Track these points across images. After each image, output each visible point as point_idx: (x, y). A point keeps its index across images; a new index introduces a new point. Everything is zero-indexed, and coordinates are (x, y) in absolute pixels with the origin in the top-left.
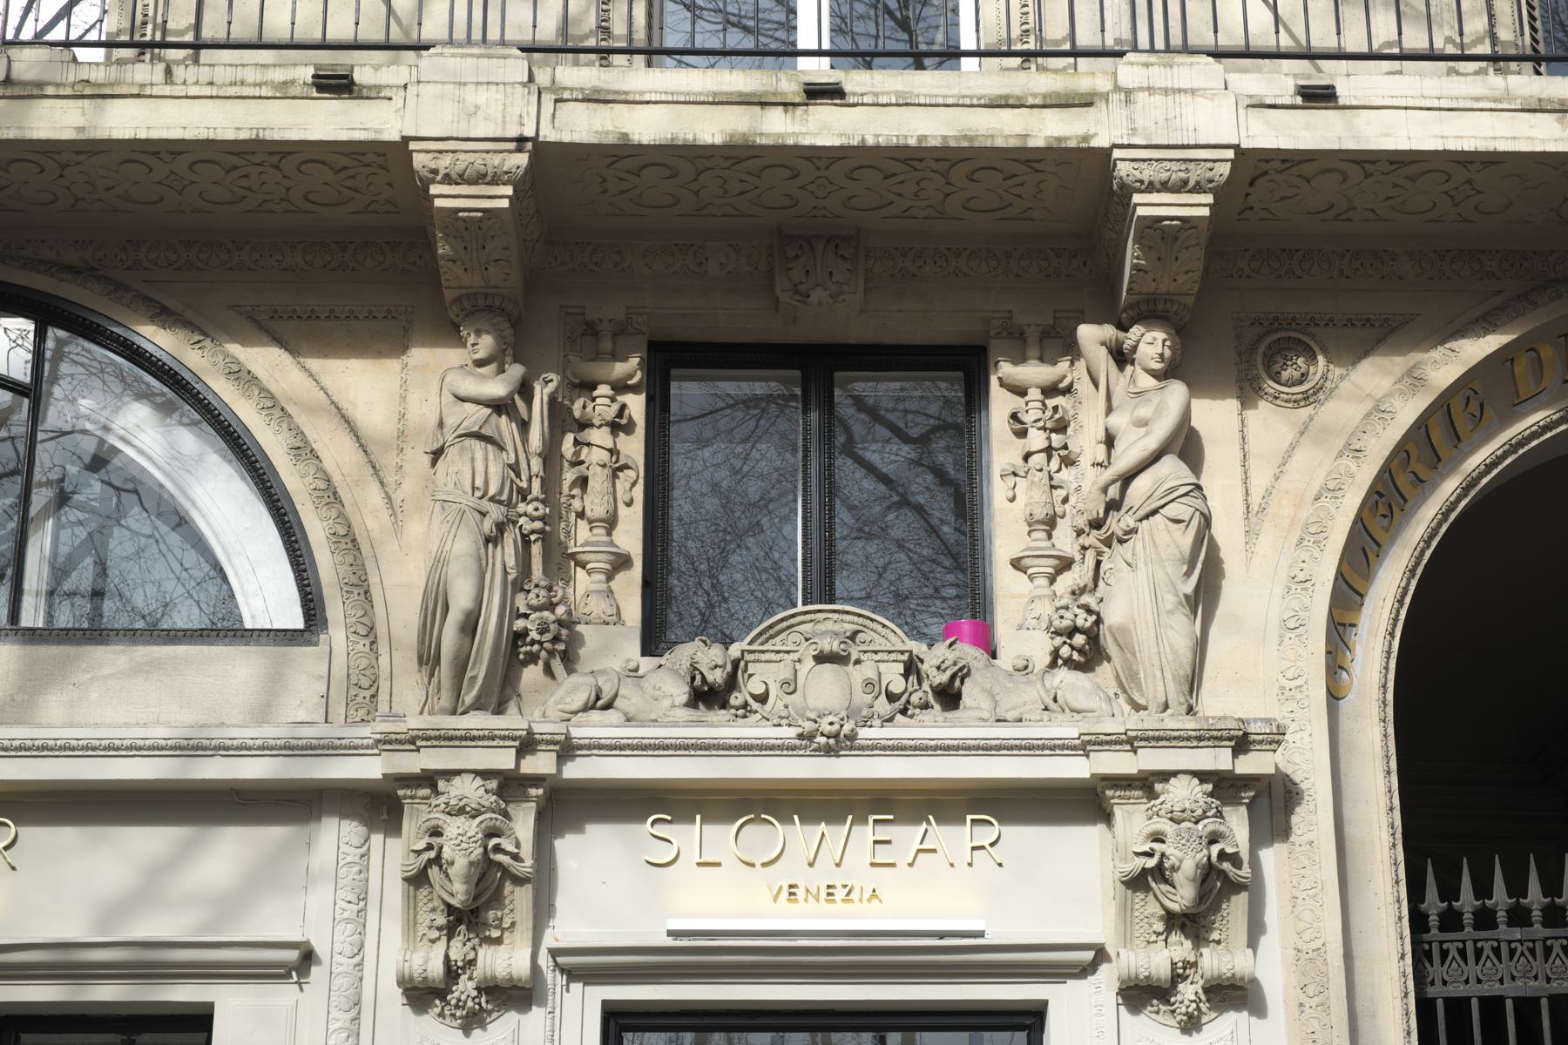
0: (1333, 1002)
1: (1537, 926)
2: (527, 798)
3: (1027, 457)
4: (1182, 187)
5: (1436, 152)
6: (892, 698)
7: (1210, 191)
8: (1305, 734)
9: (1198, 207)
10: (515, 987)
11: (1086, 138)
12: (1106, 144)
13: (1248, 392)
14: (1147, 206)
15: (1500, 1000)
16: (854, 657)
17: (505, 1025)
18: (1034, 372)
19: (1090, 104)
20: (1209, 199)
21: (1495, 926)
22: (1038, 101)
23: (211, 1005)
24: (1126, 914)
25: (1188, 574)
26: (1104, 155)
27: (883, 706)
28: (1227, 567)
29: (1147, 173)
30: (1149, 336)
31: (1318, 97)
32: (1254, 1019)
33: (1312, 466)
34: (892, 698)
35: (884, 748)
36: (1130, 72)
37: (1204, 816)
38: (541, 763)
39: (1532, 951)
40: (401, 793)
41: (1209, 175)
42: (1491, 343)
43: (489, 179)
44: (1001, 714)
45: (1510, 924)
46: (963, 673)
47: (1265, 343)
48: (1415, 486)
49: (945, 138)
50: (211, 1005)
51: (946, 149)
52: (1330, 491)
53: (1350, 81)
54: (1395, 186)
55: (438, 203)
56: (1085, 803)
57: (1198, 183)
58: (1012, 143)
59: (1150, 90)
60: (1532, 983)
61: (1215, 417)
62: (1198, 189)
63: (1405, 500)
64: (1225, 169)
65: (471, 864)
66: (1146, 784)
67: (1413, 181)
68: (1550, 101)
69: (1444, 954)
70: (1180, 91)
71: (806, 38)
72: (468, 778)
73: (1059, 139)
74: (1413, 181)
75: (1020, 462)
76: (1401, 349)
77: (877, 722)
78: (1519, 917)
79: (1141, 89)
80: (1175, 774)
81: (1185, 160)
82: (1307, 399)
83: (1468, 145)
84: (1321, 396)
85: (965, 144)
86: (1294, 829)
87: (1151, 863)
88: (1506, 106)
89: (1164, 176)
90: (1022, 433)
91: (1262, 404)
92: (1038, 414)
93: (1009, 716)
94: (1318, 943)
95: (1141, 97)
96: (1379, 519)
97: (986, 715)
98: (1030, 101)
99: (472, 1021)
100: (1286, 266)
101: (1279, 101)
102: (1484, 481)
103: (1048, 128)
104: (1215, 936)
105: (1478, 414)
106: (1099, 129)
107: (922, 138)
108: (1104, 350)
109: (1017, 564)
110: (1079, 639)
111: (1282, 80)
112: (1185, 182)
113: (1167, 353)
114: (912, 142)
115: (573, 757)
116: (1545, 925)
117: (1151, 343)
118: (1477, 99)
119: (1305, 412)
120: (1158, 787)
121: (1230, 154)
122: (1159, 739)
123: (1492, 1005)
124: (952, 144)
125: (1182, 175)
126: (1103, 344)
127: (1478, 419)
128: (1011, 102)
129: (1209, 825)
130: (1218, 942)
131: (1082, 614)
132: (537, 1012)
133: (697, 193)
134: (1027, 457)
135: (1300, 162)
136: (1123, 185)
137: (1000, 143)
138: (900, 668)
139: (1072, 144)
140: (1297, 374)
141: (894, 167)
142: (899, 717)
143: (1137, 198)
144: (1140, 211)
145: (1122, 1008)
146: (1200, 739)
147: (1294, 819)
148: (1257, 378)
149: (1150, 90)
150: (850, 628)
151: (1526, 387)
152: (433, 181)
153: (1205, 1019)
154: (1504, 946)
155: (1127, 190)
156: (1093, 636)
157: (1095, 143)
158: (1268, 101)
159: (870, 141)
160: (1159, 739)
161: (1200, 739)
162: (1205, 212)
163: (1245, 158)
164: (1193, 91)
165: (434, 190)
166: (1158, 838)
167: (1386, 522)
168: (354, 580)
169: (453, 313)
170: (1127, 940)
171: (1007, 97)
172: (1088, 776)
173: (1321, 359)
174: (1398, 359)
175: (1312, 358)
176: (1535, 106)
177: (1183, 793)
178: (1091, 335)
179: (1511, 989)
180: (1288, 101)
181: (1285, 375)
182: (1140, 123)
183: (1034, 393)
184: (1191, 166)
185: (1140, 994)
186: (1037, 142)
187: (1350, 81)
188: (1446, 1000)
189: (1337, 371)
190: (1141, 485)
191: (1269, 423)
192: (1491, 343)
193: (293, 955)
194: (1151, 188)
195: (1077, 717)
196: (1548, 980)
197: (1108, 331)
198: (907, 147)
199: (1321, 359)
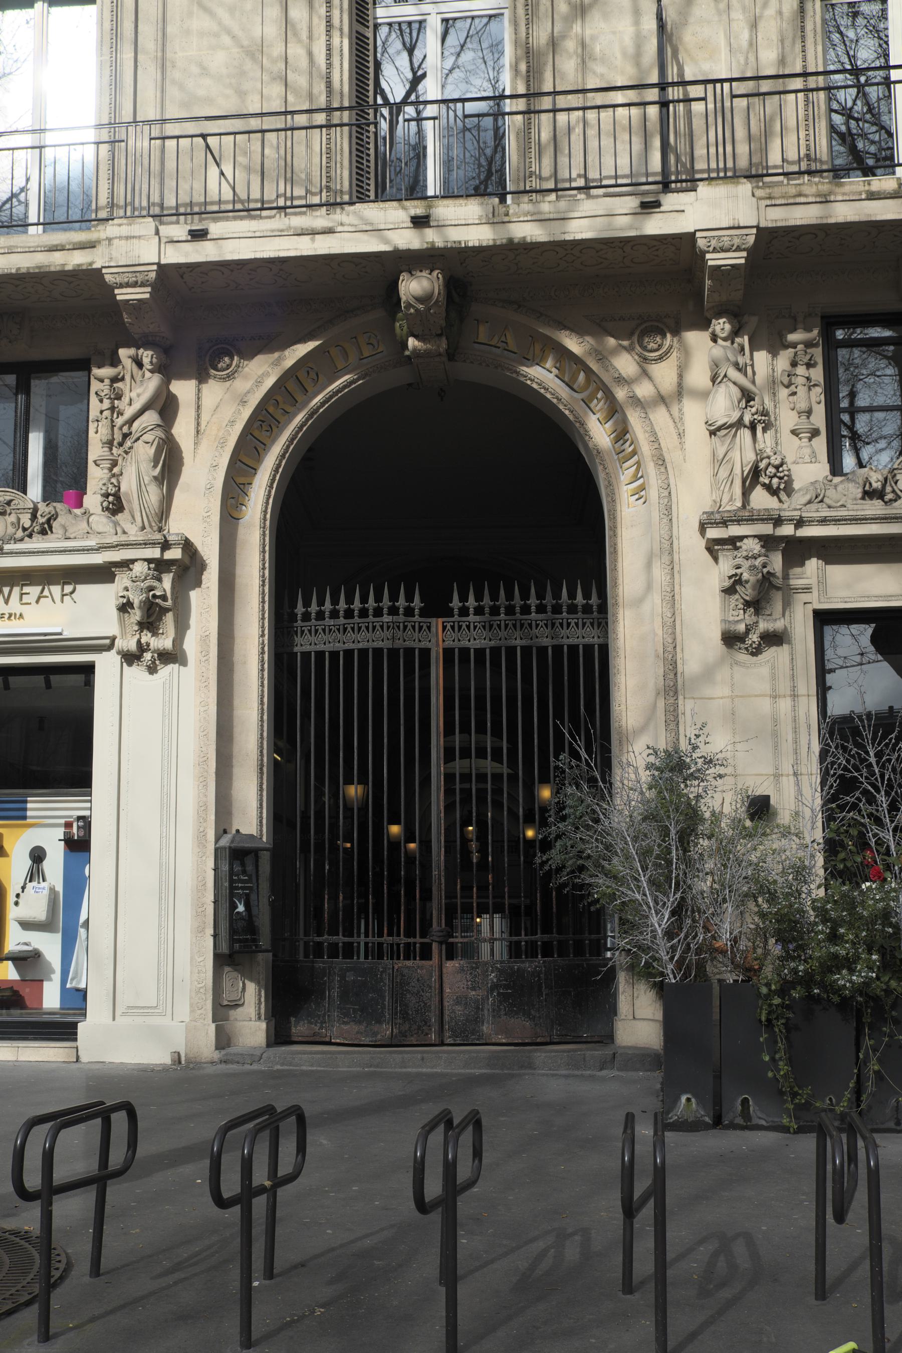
0: (211, 659)
1: (342, 618)
2: (169, 571)
3: (102, 412)
4: (135, 285)
5: (251, 259)
6: (24, 529)
7: (744, 250)
8: (209, 538)
9: (738, 259)
10: (167, 653)
11: (91, 264)
12: (692, 230)
13: (202, 377)
14: (714, 260)
15: (323, 652)
16: (8, 512)
17: (166, 671)
18: (106, 372)
19: (94, 247)
20: (744, 254)
21: (353, 617)
22: (71, 247)
23: (94, 662)
24: (122, 622)
25: (155, 466)
26: (691, 237)
27: (20, 534)
28: (185, 461)
29: (118, 280)
30: (146, 353)
31: (198, 235)
32: (181, 667)
33: (228, 412)
34: (24, 529)
35: (16, 553)
36: (111, 230)
37: (145, 579)
38: (787, 530)
39: (339, 630)
40: (113, 569)
41: (146, 278)
42: (311, 345)
43: (734, 248)
44: (68, 535)
45: (331, 618)
46: (55, 517)
47: (211, 351)
48: (284, 415)
49: (28, 268)
50: (94, 662)
51: (29, 273)
52: (232, 423)
53: (215, 229)
54: (895, 236)
55: (118, 298)
56: (103, 574)
57: (142, 282)
58: (58, 268)
59: (120, 238)
60: (337, 644)
61: (183, 389)
62: (143, 285)
63: (279, 423)
64: (153, 275)
65: (141, 602)
66: (126, 564)
67: (798, 239)
68: (307, 230)
69: (303, 632)
70: (134, 237)
71: (33, 218)
72: (751, 540)
73: (79, 265)
74: (798, 239)
75: (99, 414)
76: (271, 351)
77: (12, 542)
78: (393, 611)
79: (116, 238)
80: (136, 560)
81: (135, 272)
82: (229, 377)
83: (266, 255)
84: (236, 375)
85: (37, 271)
86: (204, 582)
87: (125, 601)
88: (286, 233)
89: (126, 280)
90: (101, 401)
91: (211, 381)
92: (106, 391)
93: (72, 536)
94: (207, 633)
95: (116, 242)
96: (264, 433)
97: (60, 536)
98: (67, 247)
99: (756, 652)
100: (202, 317)
101: (180, 239)
102: (321, 410)
103: (77, 259)
104: (161, 631)
105: (315, 378)
106: (97, 259)
107: (18, 269)
108: (130, 360)
109: (794, 432)
110: (111, 498)
111: (179, 231)
112: (136, 282)
113: (154, 360)
114: (14, 271)
115: (169, 549)
116: (421, 616)
117: (147, 356)
118: (273, 231)
119: (228, 383)
120: (131, 566)
121: (754, 231)
122: (128, 545)
123: (320, 655)
124: (31, 271)
125: (134, 279)
126: (130, 357)
127: (316, 381)
128: (304, 232)
129: (148, 583)
130: (163, 634)
131: (110, 486)
132: (785, 646)
133: (517, 264)
134: (102, 412)
135: (531, 249)
136: (701, 250)
137: (53, 269)
138: (29, 516)
139: (84, 267)
140: (224, 365)
141: (656, 243)
142: (26, 538)
143: (708, 256)
144: (710, 263)
145: (125, 664)
146: (145, 544)
147: (203, 577)
148: (206, 370)
149: (120, 238)
150: (8, 498)
151: (340, 364)
152: (708, 252)
153: (159, 668)
154: (327, 628)
155: (703, 253)
156: (117, 496)
157: (94, 266)
158: (175, 239)
159: (528, 240)
160: (128, 545)
161: (145, 544)
162: (743, 261)
163: (163, 269)
164: (139, 237)
165: (116, 291)
166: (127, 589)
167: (268, 434)
168: (653, 439)
169: (708, 315)
170: (123, 634)
171: (57, 246)
172: (727, 537)
173: (668, 335)
174: (271, 355)
175: (664, 336)
176: (299, 232)
177: (139, 569)
178: (123, 353)
179: (328, 648)
180: (184, 238)
181: (219, 366)
182: (114, 254)
183: (107, 382)
184: (138, 274)
185: (130, 658)
186: (69, 267)
187: (215, 229)
188: (420, 649)
189: (246, 363)
190: (136, 425)
191: (213, 391)
192: (311, 345)
193: (107, 641)
194: (121, 286)
195: (99, 536)
196: (344, 643)
197: (132, 351)
198: (11, 274)
199: (668, 335)
